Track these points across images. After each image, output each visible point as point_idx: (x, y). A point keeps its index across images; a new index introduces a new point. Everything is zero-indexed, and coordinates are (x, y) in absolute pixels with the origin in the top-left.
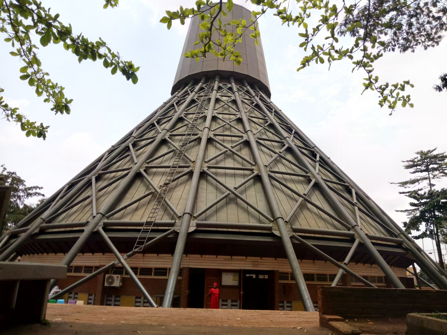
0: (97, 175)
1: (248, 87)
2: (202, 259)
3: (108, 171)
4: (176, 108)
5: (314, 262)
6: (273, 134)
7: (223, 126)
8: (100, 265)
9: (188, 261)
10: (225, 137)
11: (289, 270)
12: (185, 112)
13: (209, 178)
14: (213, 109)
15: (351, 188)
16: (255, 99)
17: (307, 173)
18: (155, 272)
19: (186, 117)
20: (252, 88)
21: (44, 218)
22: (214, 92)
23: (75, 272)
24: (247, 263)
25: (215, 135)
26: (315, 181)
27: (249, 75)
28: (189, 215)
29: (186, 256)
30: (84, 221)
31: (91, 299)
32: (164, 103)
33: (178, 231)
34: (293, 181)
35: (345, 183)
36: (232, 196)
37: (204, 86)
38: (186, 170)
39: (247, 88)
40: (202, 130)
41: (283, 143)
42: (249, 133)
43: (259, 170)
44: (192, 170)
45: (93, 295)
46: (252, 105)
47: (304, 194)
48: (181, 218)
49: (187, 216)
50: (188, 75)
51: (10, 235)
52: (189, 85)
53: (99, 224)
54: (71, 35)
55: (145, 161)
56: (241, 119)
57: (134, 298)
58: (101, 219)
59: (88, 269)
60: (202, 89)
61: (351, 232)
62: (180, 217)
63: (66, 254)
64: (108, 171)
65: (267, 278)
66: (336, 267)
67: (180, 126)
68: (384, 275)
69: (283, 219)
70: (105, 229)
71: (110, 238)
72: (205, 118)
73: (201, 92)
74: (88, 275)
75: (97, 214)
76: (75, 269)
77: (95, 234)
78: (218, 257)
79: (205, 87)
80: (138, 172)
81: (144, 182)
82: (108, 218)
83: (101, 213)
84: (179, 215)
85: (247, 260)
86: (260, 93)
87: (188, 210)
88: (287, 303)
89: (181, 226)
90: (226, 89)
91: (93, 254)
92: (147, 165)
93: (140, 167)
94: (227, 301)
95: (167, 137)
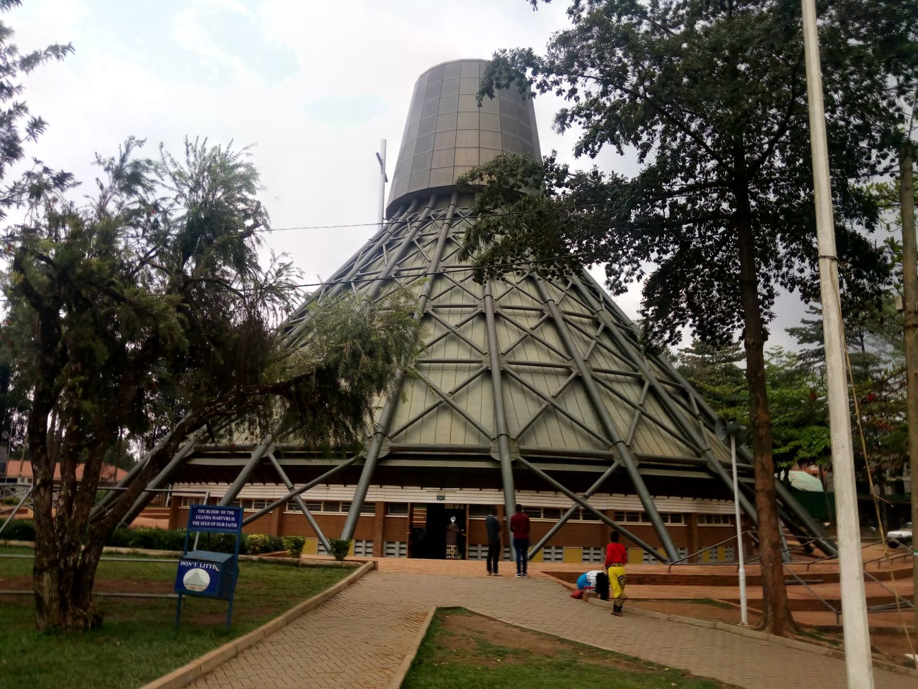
9: (383, 493)
11: (641, 508)
17: (636, 371)
34: (619, 382)
36: (551, 407)
47: (640, 405)
50: (406, 193)
59: (260, 502)
60: (428, 219)
68: (643, 509)
70: (277, 454)
71: (283, 467)
74: (258, 511)
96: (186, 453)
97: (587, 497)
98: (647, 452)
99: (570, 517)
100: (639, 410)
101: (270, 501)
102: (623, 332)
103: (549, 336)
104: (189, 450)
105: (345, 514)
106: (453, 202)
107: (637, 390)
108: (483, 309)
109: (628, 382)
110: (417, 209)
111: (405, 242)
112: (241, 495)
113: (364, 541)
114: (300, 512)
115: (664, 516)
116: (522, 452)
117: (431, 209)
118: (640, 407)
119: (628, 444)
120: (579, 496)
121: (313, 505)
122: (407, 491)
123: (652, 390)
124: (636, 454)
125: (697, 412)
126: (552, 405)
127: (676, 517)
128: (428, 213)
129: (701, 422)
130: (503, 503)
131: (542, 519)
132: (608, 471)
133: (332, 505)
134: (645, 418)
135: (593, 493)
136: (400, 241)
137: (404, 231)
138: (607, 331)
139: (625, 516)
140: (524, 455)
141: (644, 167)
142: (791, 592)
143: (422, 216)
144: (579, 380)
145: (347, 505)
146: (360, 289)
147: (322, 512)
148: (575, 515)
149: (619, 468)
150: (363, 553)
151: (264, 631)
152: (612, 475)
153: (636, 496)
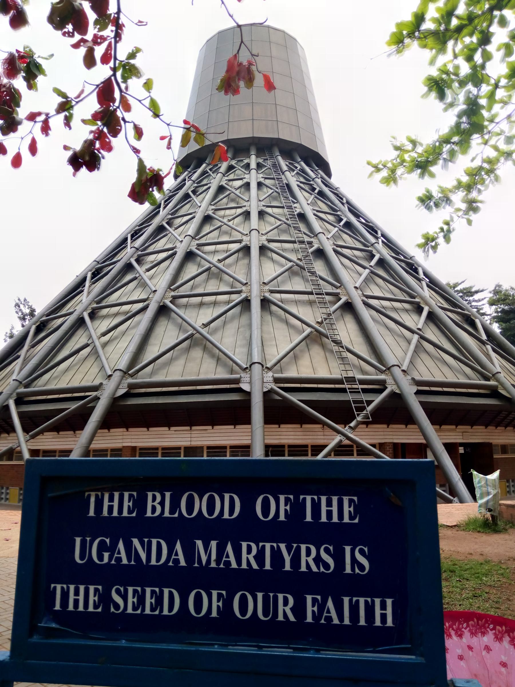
1: (302, 163)
2: (406, 430)
3: (103, 304)
4: (195, 199)
5: (440, 428)
6: (350, 236)
10: (283, 244)
11: (420, 440)
12: (213, 207)
13: (274, 308)
14: (209, 202)
15: (474, 318)
16: (315, 183)
19: (214, 213)
20: (308, 165)
22: (253, 172)
24: (457, 434)
25: (270, 241)
26: (428, 310)
27: (303, 143)
29: (366, 427)
35: (464, 311)
37: (233, 163)
38: (237, 298)
40: (247, 234)
41: (371, 252)
42: (321, 236)
43: (348, 294)
44: (247, 297)
46: (313, 192)
47: (419, 329)
48: (248, 370)
52: (206, 162)
54: (36, 81)
55: (169, 287)
56: (303, 214)
57: (18, 490)
61: (492, 383)
62: (247, 368)
64: (103, 304)
65: (463, 452)
66: (335, 433)
67: (208, 231)
69: (400, 368)
72: (247, 215)
76: (185, 452)
78: (282, 426)
79: (235, 165)
81: (174, 319)
82: (132, 376)
83: (120, 370)
85: (458, 430)
86: (319, 173)
90: (240, 168)
91: (109, 431)
92: (173, 294)
93: (163, 297)
95: (194, 249)
98: (427, 377)
102: (403, 265)
107: (415, 317)
108: (248, 243)
116: (277, 381)
118: (418, 331)
119: (404, 368)
122: (133, 433)
123: (432, 317)
124: (413, 379)
125: (484, 337)
126: (317, 330)
128: (206, 167)
129: (489, 347)
132: (378, 399)
134: (425, 344)
140: (282, 385)
142: (14, 567)
153: (416, 426)
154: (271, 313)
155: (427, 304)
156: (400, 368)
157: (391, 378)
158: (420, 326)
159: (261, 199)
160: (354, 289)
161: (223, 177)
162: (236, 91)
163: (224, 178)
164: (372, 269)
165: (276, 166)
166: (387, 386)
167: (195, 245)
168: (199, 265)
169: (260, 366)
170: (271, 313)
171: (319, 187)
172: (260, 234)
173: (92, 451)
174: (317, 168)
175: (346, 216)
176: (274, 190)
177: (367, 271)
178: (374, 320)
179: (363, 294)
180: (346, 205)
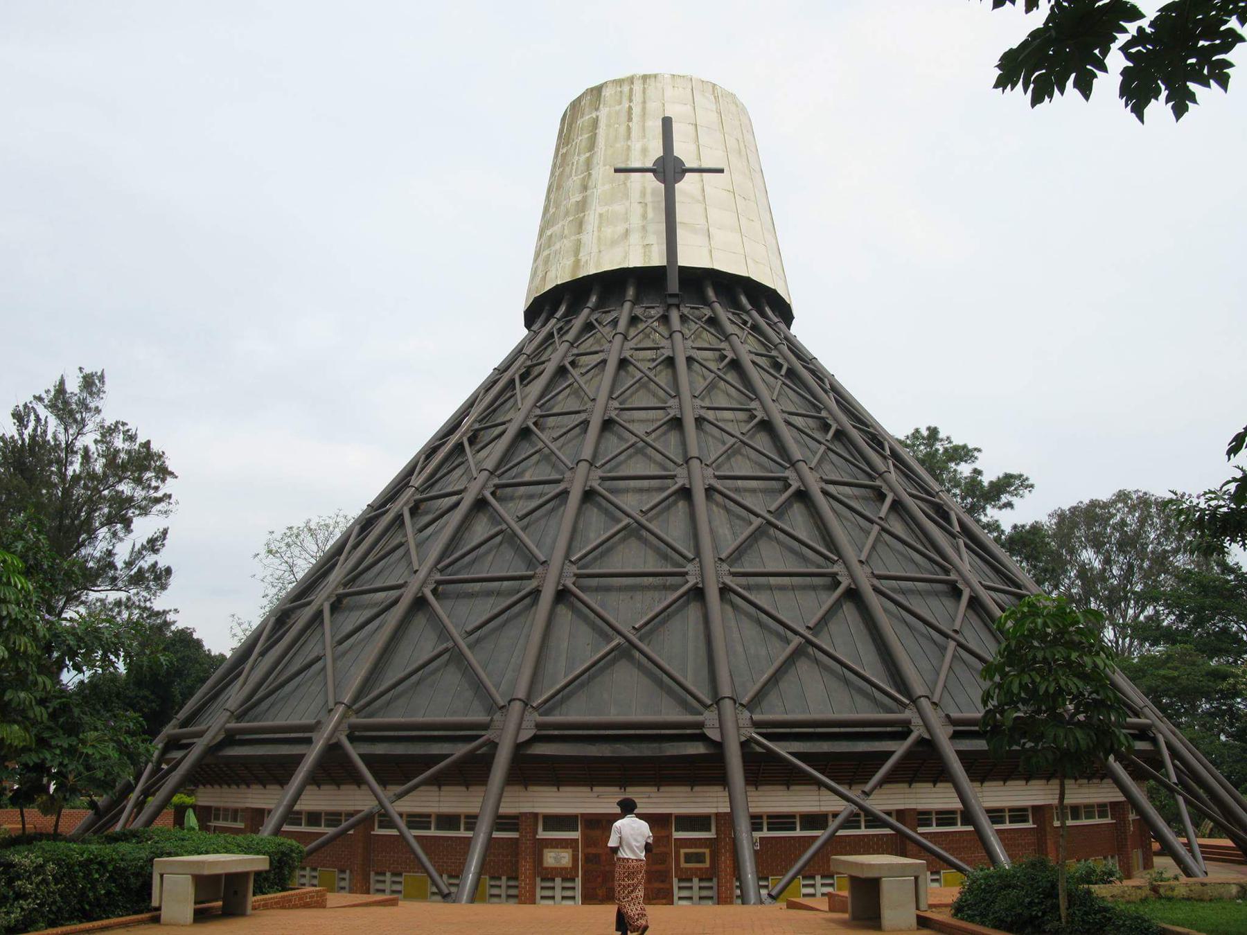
0: (332, 600)
1: (754, 313)
7: (633, 445)
8: (355, 811)
11: (956, 805)
18: (326, 820)
21: (232, 709)
23: (309, 823)
28: (523, 704)
30: (308, 720)
31: (344, 879)
32: (495, 369)
33: (497, 740)
39: (713, 310)
45: (348, 872)
49: (517, 706)
50: (567, 278)
51: (164, 742)
53: (340, 728)
58: (488, 480)
59: (334, 818)
60: (589, 327)
62: (503, 707)
63: (285, 787)
68: (960, 806)
70: (351, 738)
73: (589, 337)
74: (331, 831)
75: (336, 704)
77: (333, 749)
80: (420, 595)
84: (502, 704)
87: (521, 694)
88: (823, 877)
89: (502, 729)
94: (384, 874)
96: (214, 738)
97: (867, 794)
99: (843, 826)
100: (954, 640)
101: (350, 815)
103: (798, 523)
104: (217, 734)
105: (469, 834)
106: (631, 292)
107: (949, 603)
109: (936, 594)
110: (573, 311)
111: (550, 368)
112: (304, 805)
113: (504, 878)
114: (394, 832)
115: (996, 815)
116: (756, 725)
117: (593, 310)
120: (854, 793)
121: (418, 821)
124: (948, 716)
127: (1018, 814)
130: (728, 810)
131: (798, 833)
133: (448, 821)
135: (881, 784)
136: (542, 367)
137: (550, 349)
138: (898, 507)
139: (934, 817)
140: (764, 731)
141: (1050, 5)
143: (578, 323)
144: (853, 595)
145: (471, 821)
146: (479, 451)
147: (433, 832)
148: (851, 822)
149: (921, 741)
150: (504, 896)
151: (652, 611)
152: (908, 755)
153: (950, 785)
154: (706, 432)
155: (892, 489)
156: (929, 699)
157: (917, 715)
158: (882, 514)
159: (723, 556)
160: (858, 564)
161: (623, 345)
162: (929, 429)
163: (626, 343)
164: (882, 523)
165: (713, 321)
166: (912, 728)
167: (597, 477)
168: (621, 438)
169: (732, 702)
170: (706, 432)
171: (789, 363)
172: (737, 705)
173: (323, 814)
174: (776, 320)
175: (836, 420)
176: (737, 437)
177: (823, 448)
178: (885, 610)
179: (872, 573)
180: (831, 394)
